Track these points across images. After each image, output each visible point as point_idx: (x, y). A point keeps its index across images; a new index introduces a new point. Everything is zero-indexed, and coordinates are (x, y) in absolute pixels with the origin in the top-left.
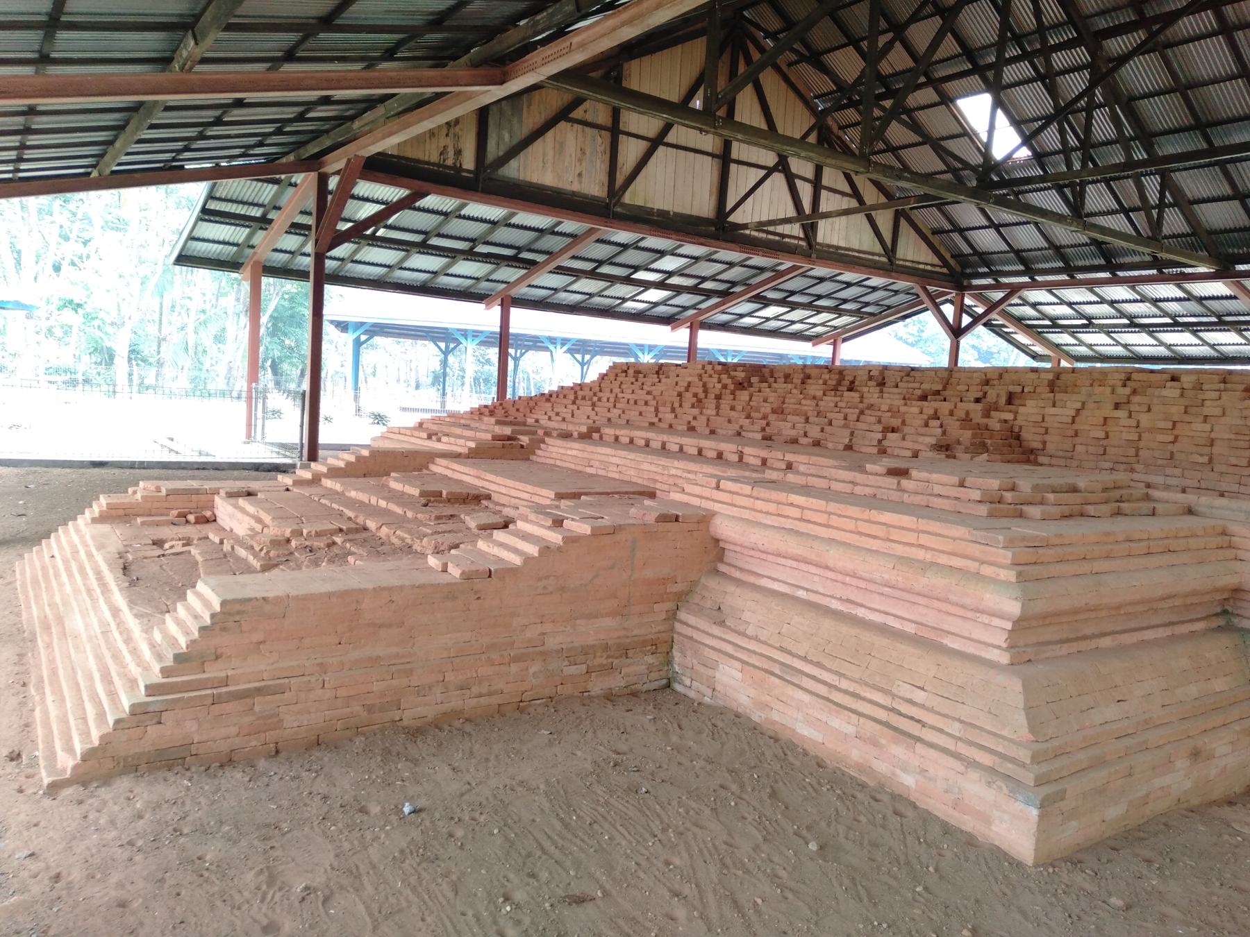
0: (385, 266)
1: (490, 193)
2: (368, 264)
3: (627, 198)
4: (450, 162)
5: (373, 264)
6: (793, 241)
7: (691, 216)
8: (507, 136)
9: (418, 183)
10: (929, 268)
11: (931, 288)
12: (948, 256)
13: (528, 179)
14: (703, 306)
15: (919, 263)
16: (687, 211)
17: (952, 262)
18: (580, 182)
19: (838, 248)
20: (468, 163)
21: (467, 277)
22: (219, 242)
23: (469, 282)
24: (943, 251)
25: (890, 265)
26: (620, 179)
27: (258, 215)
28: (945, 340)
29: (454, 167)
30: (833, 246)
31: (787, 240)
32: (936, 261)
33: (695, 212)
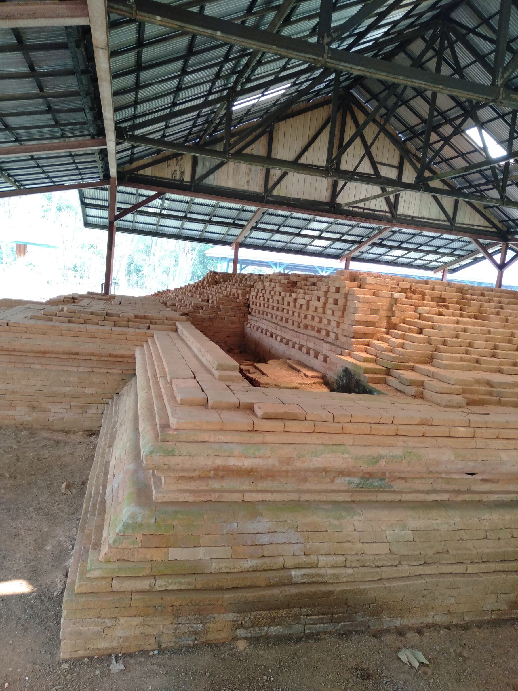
0: (285, 242)
1: (196, 192)
2: (211, 233)
3: (275, 192)
4: (177, 178)
5: (260, 239)
6: (381, 213)
7: (314, 201)
8: (208, 164)
9: (160, 188)
10: (481, 228)
11: (481, 241)
12: (496, 222)
13: (219, 184)
14: (352, 249)
15: (473, 225)
16: (312, 198)
17: (500, 225)
18: (248, 185)
19: (413, 217)
20: (187, 177)
21: (339, 249)
22: (99, 217)
23: (221, 236)
24: (492, 218)
25: (451, 226)
26: (271, 183)
27: (184, 215)
28: (495, 271)
29: (180, 180)
30: (409, 216)
31: (377, 213)
32: (487, 224)
33: (317, 199)
